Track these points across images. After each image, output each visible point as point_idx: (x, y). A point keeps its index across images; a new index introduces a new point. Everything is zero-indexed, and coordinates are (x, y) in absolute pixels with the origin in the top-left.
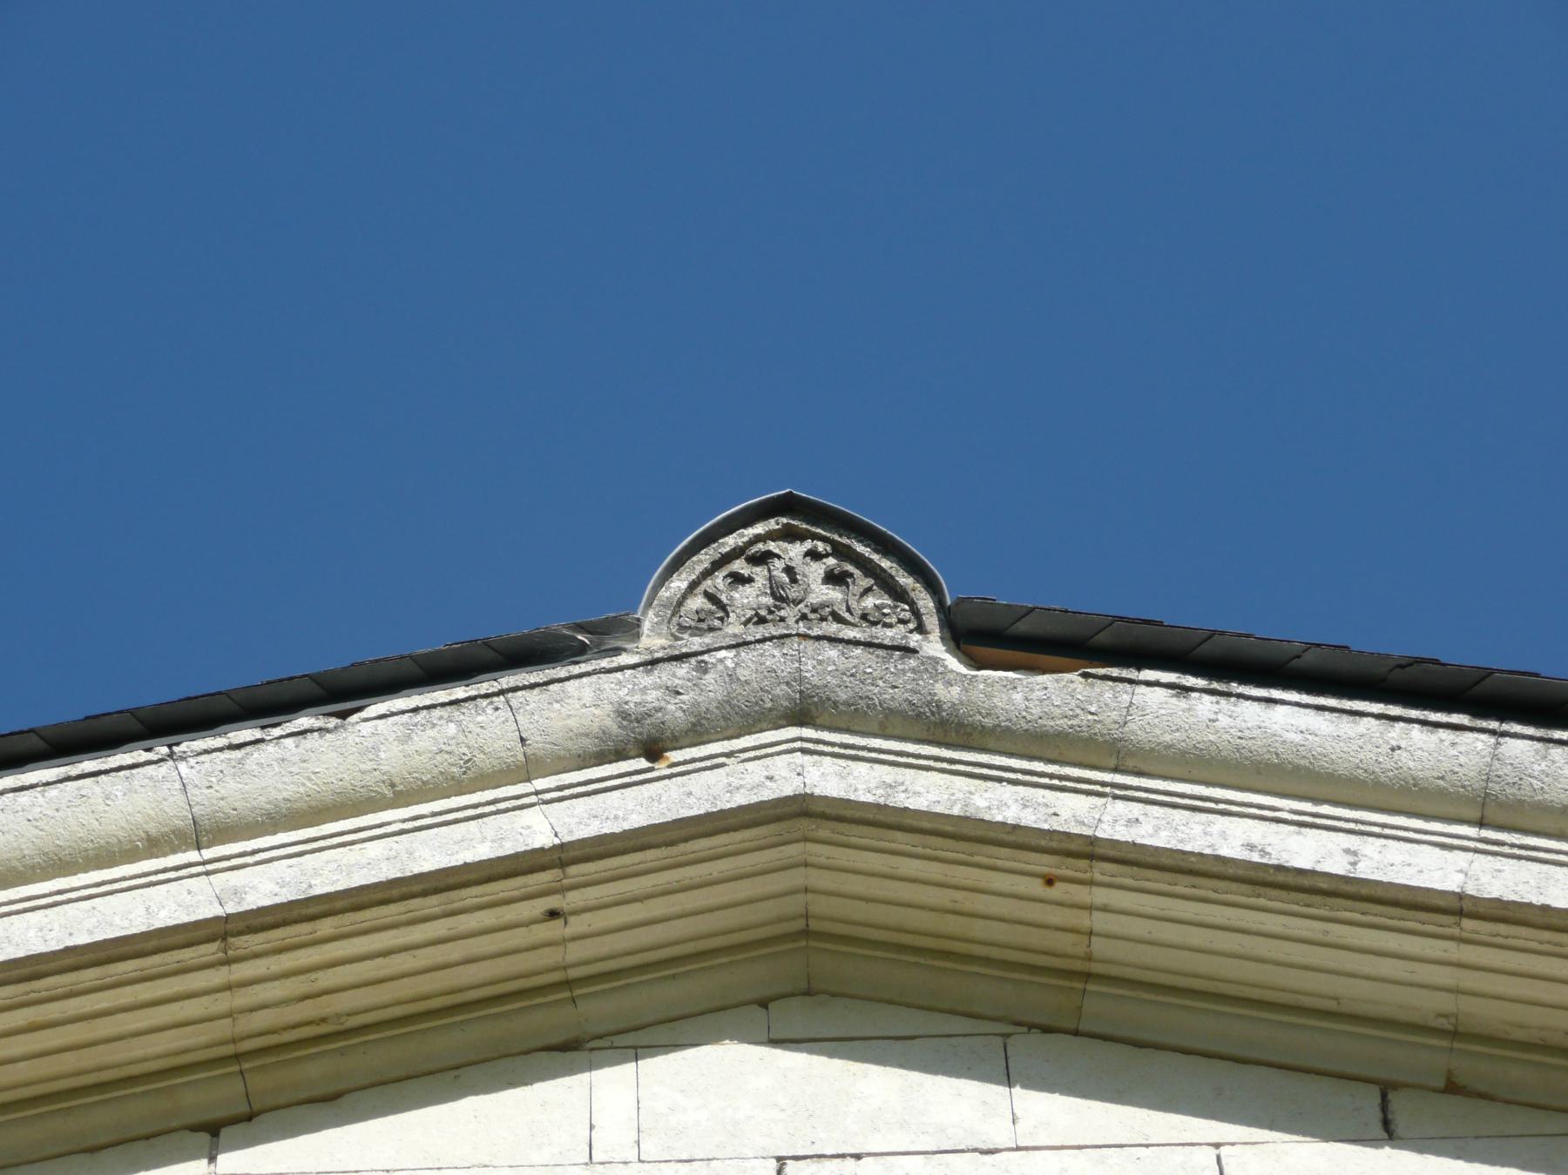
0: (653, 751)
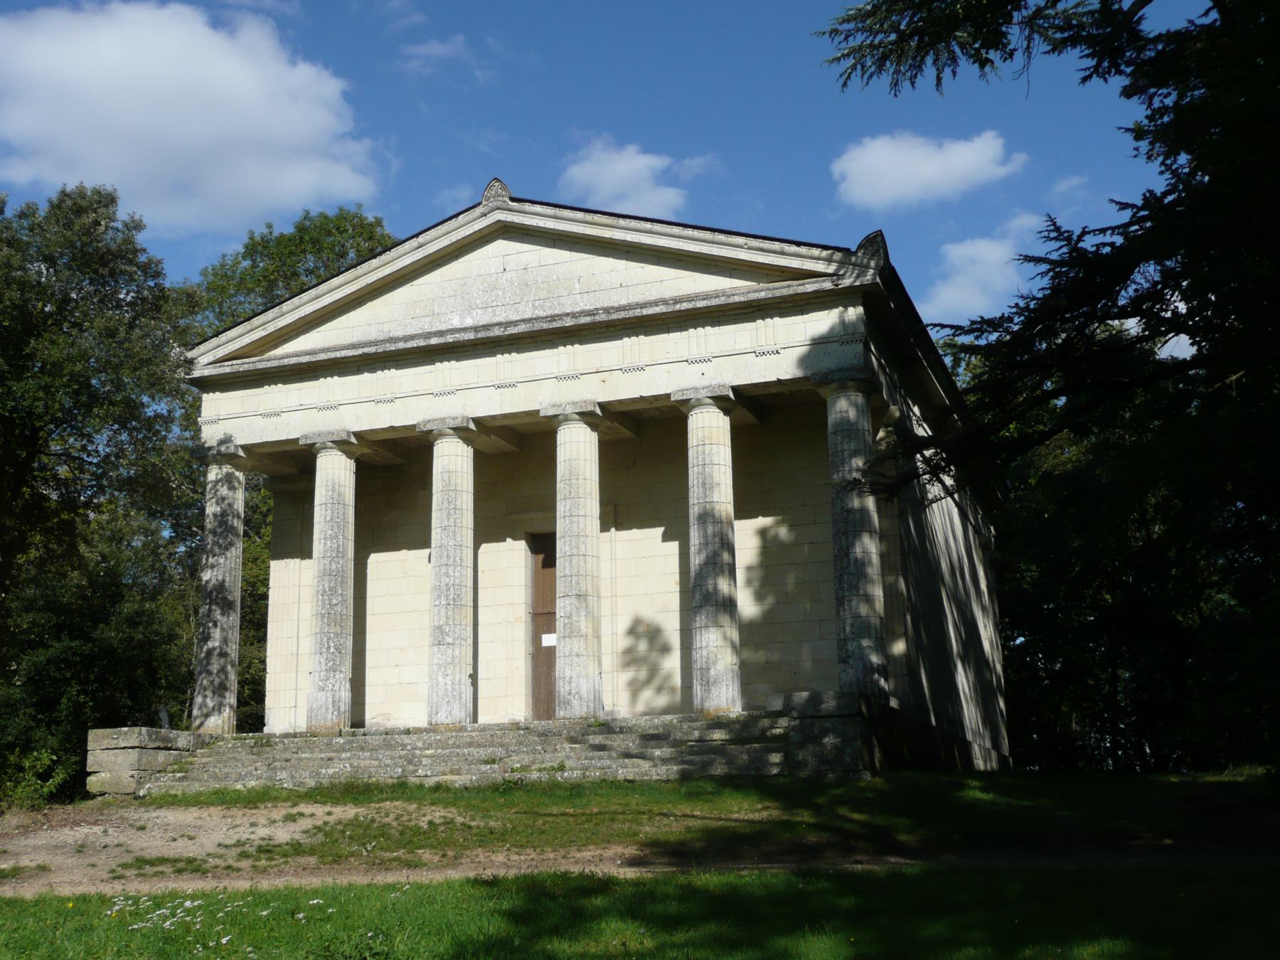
0: (485, 216)
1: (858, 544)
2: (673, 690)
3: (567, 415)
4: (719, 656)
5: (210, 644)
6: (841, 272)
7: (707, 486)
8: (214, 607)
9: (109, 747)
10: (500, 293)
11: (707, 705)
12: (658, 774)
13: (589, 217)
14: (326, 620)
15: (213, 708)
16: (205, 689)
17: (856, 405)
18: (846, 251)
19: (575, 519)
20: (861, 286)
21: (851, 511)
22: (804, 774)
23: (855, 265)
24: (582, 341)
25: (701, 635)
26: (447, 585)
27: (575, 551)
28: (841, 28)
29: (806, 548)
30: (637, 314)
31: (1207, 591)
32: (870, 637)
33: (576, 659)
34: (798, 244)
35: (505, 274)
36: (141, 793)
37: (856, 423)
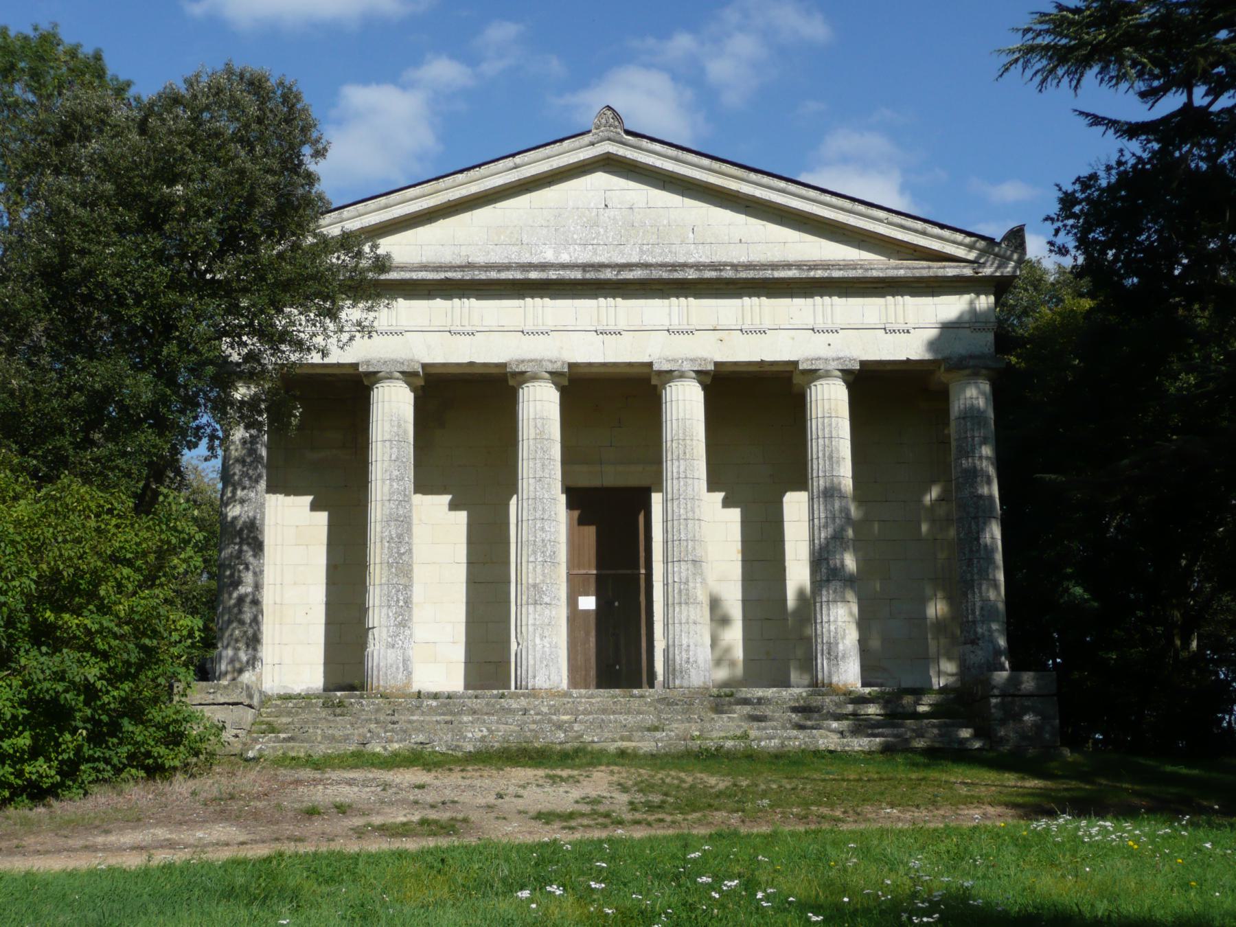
0: (593, 145)
1: (987, 530)
2: (732, 664)
3: (683, 372)
4: (847, 632)
5: (242, 590)
6: (982, 261)
7: (832, 459)
8: (245, 548)
9: (203, 702)
10: (602, 231)
11: (835, 680)
12: (860, 745)
13: (716, 165)
14: (394, 570)
15: (248, 662)
16: (237, 641)
17: (984, 394)
18: (990, 241)
19: (690, 481)
20: (1002, 276)
21: (981, 497)
22: (1006, 748)
23: (996, 255)
24: (697, 295)
25: (829, 609)
26: (543, 541)
27: (690, 515)
28: (1035, 27)
29: (876, 526)
30: (768, 276)
31: (1065, 584)
32: (998, 621)
33: (692, 627)
34: (942, 227)
35: (607, 210)
36: (251, 754)
37: (984, 412)
